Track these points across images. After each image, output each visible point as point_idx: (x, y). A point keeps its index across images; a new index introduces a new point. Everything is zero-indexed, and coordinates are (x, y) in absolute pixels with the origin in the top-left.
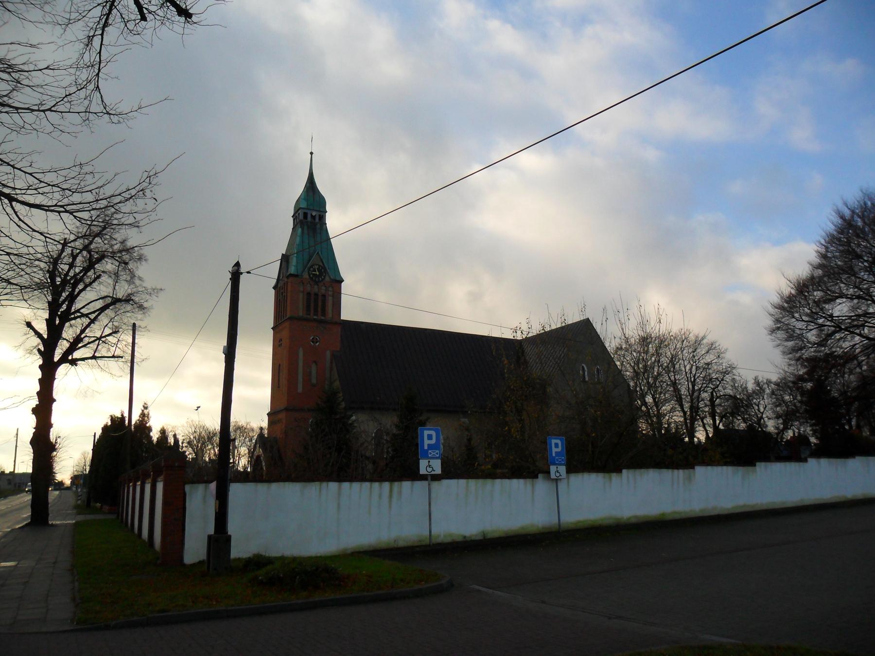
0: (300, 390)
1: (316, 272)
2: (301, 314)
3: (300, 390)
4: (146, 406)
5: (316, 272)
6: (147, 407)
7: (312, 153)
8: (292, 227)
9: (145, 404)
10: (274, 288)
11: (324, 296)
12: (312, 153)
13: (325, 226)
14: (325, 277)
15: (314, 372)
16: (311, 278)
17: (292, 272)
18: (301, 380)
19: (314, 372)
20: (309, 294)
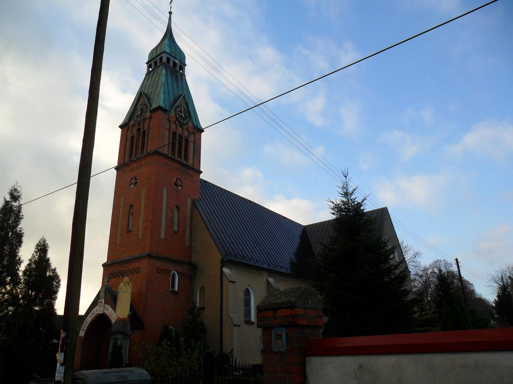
0: (163, 236)
1: (182, 113)
2: (166, 152)
3: (163, 236)
4: (16, 194)
5: (182, 113)
6: (19, 197)
7: (170, 13)
8: (146, 73)
9: (16, 190)
10: (121, 127)
11: (187, 140)
12: (170, 13)
13: (184, 77)
14: (189, 121)
15: (176, 219)
16: (177, 118)
17: (162, 104)
18: (164, 223)
19: (176, 219)
20: (174, 133)
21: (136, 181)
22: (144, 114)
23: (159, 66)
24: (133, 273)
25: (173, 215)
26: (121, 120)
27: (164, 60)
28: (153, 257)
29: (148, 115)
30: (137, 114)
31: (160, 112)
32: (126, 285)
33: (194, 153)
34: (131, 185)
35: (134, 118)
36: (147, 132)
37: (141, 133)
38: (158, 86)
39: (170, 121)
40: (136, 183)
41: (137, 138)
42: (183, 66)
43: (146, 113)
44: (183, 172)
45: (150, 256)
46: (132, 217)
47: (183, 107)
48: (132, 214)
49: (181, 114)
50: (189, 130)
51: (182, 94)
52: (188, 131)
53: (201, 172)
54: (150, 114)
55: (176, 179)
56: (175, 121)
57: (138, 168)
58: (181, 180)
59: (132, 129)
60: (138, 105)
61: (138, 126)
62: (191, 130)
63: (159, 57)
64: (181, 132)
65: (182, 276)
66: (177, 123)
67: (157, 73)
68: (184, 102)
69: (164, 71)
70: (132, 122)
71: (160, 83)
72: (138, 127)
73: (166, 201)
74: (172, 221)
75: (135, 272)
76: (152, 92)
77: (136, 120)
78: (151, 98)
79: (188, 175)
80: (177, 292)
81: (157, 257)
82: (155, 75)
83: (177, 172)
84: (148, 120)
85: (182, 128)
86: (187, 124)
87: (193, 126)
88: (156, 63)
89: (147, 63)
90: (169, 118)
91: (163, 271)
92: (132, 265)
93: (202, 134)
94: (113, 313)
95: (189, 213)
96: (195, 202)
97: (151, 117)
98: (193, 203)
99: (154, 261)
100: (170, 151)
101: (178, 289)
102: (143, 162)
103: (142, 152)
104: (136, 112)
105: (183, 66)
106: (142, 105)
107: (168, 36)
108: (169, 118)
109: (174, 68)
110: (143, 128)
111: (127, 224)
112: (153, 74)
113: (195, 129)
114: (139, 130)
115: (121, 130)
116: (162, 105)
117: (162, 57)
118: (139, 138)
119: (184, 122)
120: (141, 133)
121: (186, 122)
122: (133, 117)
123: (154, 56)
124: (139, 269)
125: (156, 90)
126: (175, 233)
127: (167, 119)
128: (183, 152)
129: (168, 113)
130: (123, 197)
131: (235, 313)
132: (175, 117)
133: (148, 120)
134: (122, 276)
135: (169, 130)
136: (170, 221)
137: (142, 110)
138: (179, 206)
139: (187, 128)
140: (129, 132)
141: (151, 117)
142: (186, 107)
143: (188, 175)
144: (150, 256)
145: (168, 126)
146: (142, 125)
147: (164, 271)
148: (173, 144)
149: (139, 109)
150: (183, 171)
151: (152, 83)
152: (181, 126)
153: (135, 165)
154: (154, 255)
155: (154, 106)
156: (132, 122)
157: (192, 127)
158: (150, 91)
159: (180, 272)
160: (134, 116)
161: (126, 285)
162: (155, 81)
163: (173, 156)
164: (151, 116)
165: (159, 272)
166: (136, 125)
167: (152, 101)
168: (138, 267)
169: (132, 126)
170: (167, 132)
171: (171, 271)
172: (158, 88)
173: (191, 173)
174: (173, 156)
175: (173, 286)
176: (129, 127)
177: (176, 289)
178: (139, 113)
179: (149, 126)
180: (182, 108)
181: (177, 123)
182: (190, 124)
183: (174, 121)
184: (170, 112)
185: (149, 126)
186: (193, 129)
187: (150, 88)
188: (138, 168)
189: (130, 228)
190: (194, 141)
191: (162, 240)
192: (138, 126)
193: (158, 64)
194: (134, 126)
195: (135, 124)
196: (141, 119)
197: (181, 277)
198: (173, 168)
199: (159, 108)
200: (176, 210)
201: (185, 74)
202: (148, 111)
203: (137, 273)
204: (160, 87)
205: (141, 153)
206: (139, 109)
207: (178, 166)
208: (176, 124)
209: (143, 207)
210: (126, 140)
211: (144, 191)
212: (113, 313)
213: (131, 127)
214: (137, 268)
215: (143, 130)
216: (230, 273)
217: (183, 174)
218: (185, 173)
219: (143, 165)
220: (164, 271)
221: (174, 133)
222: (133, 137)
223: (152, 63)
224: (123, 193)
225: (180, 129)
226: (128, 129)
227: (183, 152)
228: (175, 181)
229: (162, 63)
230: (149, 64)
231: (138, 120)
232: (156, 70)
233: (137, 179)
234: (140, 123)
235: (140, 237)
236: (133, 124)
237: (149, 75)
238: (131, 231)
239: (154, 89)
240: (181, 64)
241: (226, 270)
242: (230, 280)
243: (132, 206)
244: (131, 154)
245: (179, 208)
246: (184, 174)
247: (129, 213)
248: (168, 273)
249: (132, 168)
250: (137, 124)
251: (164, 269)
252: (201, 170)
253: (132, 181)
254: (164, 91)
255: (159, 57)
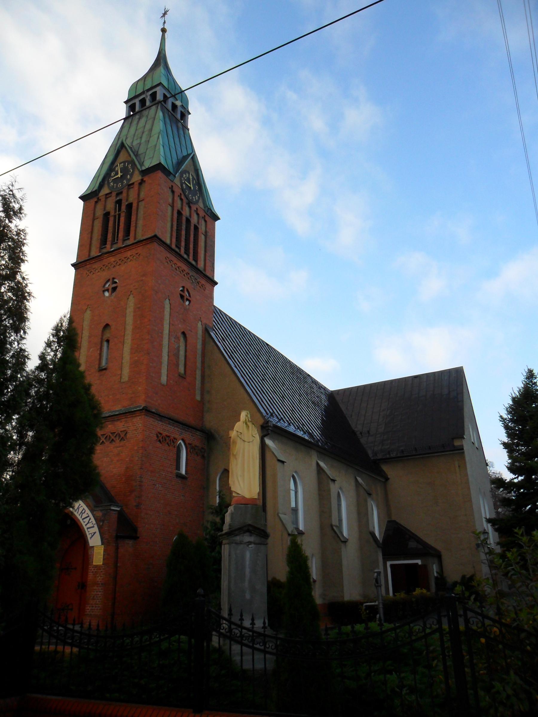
0: (164, 379)
1: (190, 184)
7: (164, 31)
11: (196, 228)
16: (183, 189)
19: (182, 353)
20: (179, 213)
21: (114, 285)
22: (129, 176)
23: (149, 107)
24: (113, 440)
25: (179, 347)
26: (83, 187)
27: (159, 97)
28: (152, 412)
29: (137, 178)
30: (114, 176)
31: (160, 174)
32: (250, 428)
33: (205, 251)
34: (104, 291)
35: (109, 183)
36: (135, 205)
37: (123, 208)
38: (152, 135)
39: (173, 192)
40: (114, 289)
41: (115, 216)
42: (185, 114)
43: (132, 175)
44: (191, 278)
45: (146, 411)
46: (108, 347)
47: (192, 175)
48: (108, 341)
49: (189, 185)
50: (199, 212)
51: (192, 153)
52: (198, 214)
53: (216, 283)
54: (140, 178)
55: (181, 289)
56: (181, 194)
57: (118, 264)
58: (189, 290)
59: (106, 201)
60: (117, 163)
61: (116, 197)
62: (202, 214)
63: (150, 92)
64: (188, 214)
65: (191, 450)
66: (183, 197)
67: (147, 116)
68: (192, 167)
69: (160, 114)
70: (105, 190)
71: (156, 130)
72: (118, 198)
73: (168, 321)
74: (177, 356)
75: (117, 438)
76: (140, 144)
77: (113, 186)
78: (140, 152)
79: (199, 284)
80: (184, 476)
81: (157, 414)
82: (143, 120)
83: (184, 276)
84: (136, 187)
85: (190, 207)
86: (197, 202)
87: (205, 207)
88: (143, 102)
89: (126, 102)
90: (172, 186)
91: (165, 440)
92: (110, 426)
93: (216, 222)
94: (84, 509)
95: (199, 346)
96: (208, 329)
97: (142, 182)
98: (206, 331)
99: (153, 420)
100: (174, 240)
101: (186, 471)
102: (128, 254)
103: (125, 239)
104: (112, 174)
105: (186, 114)
106: (124, 162)
107: (163, 65)
108: (172, 186)
109: (172, 112)
110: (127, 200)
111: (98, 357)
112: (139, 119)
113: (208, 213)
114: (119, 202)
115: (83, 202)
116: (163, 162)
117: (156, 92)
118: (119, 215)
119: (192, 198)
120: (123, 208)
121: (196, 199)
122: (106, 182)
123: (140, 91)
124: (127, 433)
125: (149, 141)
126: (183, 377)
127: (170, 188)
128: (191, 246)
129: (171, 177)
130: (88, 312)
131: (285, 515)
132: (180, 186)
133: (136, 187)
134: (110, 443)
135: (173, 207)
136: (174, 354)
137: (125, 170)
138: (186, 332)
139: (197, 209)
140: (100, 206)
141: (142, 182)
142: (195, 175)
143: (199, 284)
144: (146, 411)
145: (170, 200)
146: (124, 195)
147: (167, 438)
148: (179, 230)
149: (118, 169)
150: (192, 277)
151: (140, 131)
152: (189, 204)
153: (112, 259)
154: (153, 410)
155: (148, 164)
156: (105, 190)
157: (203, 208)
158: (135, 143)
159: (189, 444)
160: (108, 181)
161: (249, 427)
162: (144, 129)
163: (177, 250)
164: (142, 180)
165: (160, 441)
166: (114, 194)
167: (142, 157)
168: (123, 429)
169: (104, 196)
170: (170, 208)
171: (176, 439)
172: (151, 139)
173: (203, 282)
174: (177, 250)
175: (178, 467)
176: (98, 198)
177: (183, 471)
178: (119, 175)
179: (139, 195)
180: (190, 175)
181: (183, 197)
182: (201, 205)
183: (179, 194)
184: (175, 176)
185: (139, 195)
186: (205, 212)
187: (135, 138)
188: (118, 264)
189: (104, 363)
190: (206, 232)
191: (163, 385)
192: (116, 197)
193: (148, 103)
194: (107, 196)
195: (111, 193)
196: (122, 184)
197: (190, 451)
198: (177, 269)
199: (159, 167)
200: (182, 339)
201: (189, 127)
202: (137, 173)
203: (123, 439)
204: (156, 136)
205: (124, 240)
206: (118, 169)
207: (183, 266)
208: (181, 199)
209: (129, 327)
210: (94, 219)
211: (131, 302)
212: (84, 509)
213: (103, 199)
214: (121, 431)
215: (127, 203)
216: (276, 447)
217: (192, 281)
218: (194, 281)
219: (117, 262)
220: (167, 438)
221: (179, 213)
222: (107, 215)
223: (137, 101)
224: (88, 305)
225: (187, 209)
226: (96, 202)
227: (191, 246)
228: (181, 290)
229: (156, 102)
230: (130, 103)
231: (117, 186)
232: (145, 113)
233: (116, 283)
234: (120, 191)
235: (125, 378)
236: (106, 195)
237: (130, 120)
238: (105, 369)
239: (143, 140)
240: (183, 111)
241: (269, 442)
242: (279, 459)
243: (107, 326)
244: (104, 241)
245: (187, 336)
246: (192, 281)
247: (102, 339)
248: (172, 444)
249: (106, 264)
250: (116, 193)
251: (166, 436)
252: (215, 279)
253: (107, 286)
254: (163, 143)
255: (150, 92)
